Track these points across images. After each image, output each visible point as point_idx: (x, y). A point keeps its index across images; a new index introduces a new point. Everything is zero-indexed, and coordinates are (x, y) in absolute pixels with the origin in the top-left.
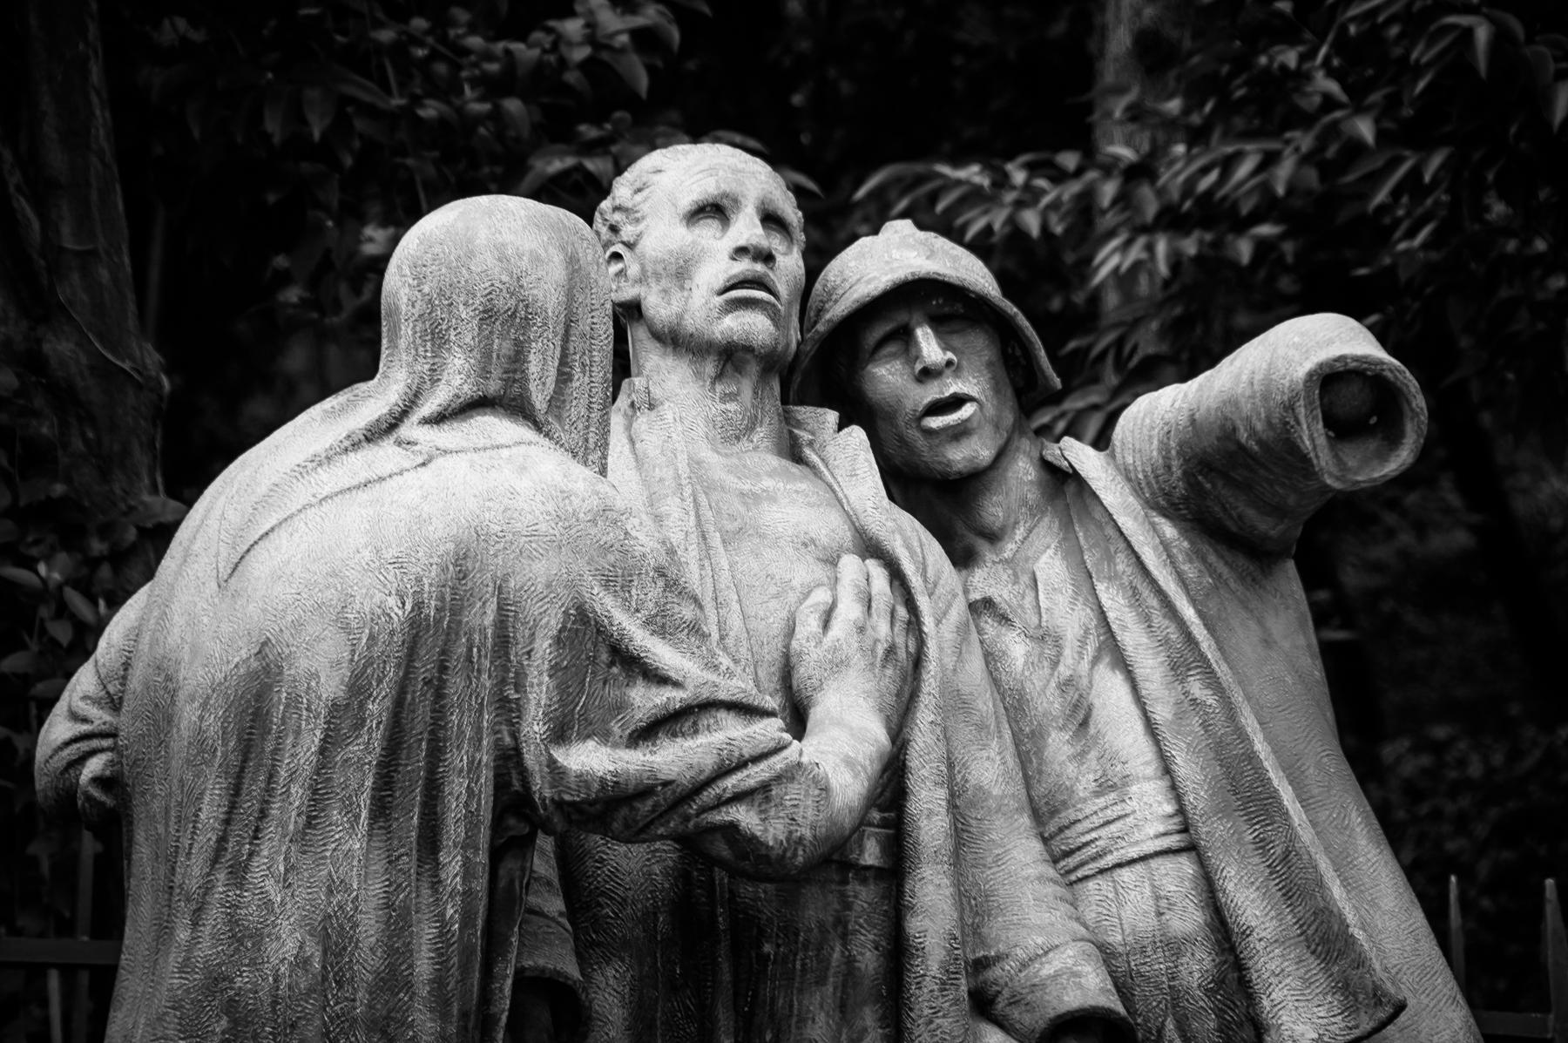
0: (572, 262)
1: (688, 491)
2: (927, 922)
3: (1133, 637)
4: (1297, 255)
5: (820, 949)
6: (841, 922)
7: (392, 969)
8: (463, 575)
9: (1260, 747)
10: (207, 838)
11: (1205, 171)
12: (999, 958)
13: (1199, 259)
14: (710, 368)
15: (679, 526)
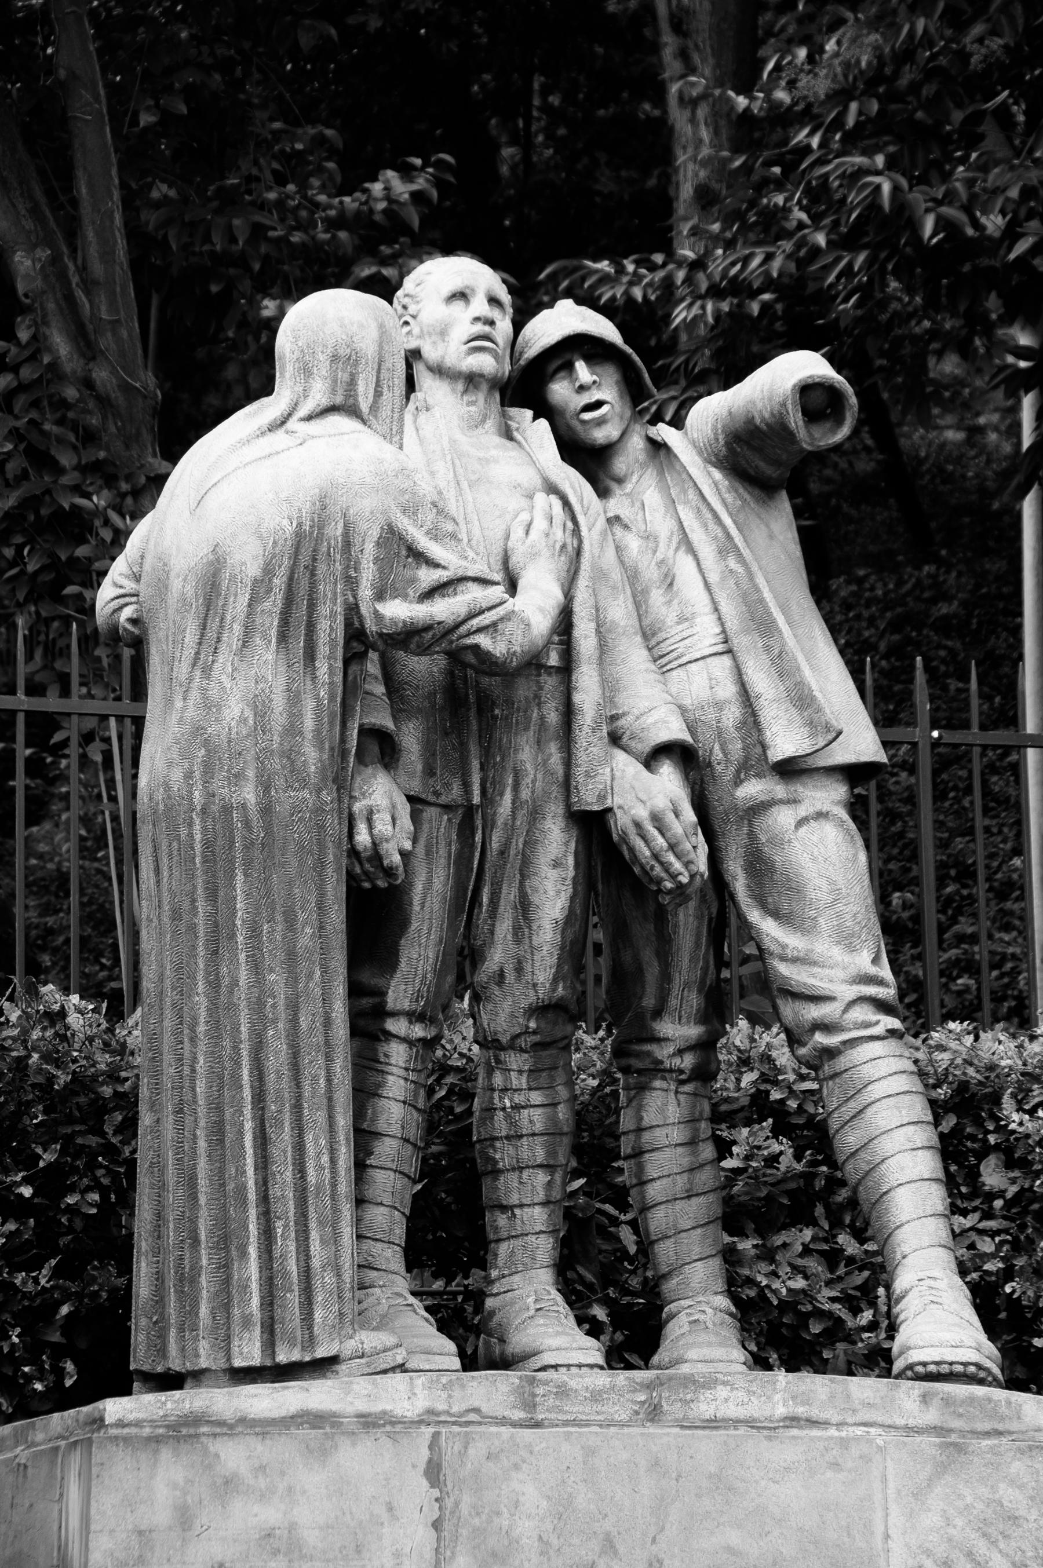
0: (381, 326)
1: (449, 458)
2: (584, 696)
3: (698, 536)
4: (783, 311)
5: (526, 712)
6: (537, 697)
7: (292, 724)
8: (324, 507)
9: (767, 595)
10: (189, 652)
11: (733, 264)
12: (624, 714)
13: (730, 314)
14: (460, 386)
15: (444, 476)
